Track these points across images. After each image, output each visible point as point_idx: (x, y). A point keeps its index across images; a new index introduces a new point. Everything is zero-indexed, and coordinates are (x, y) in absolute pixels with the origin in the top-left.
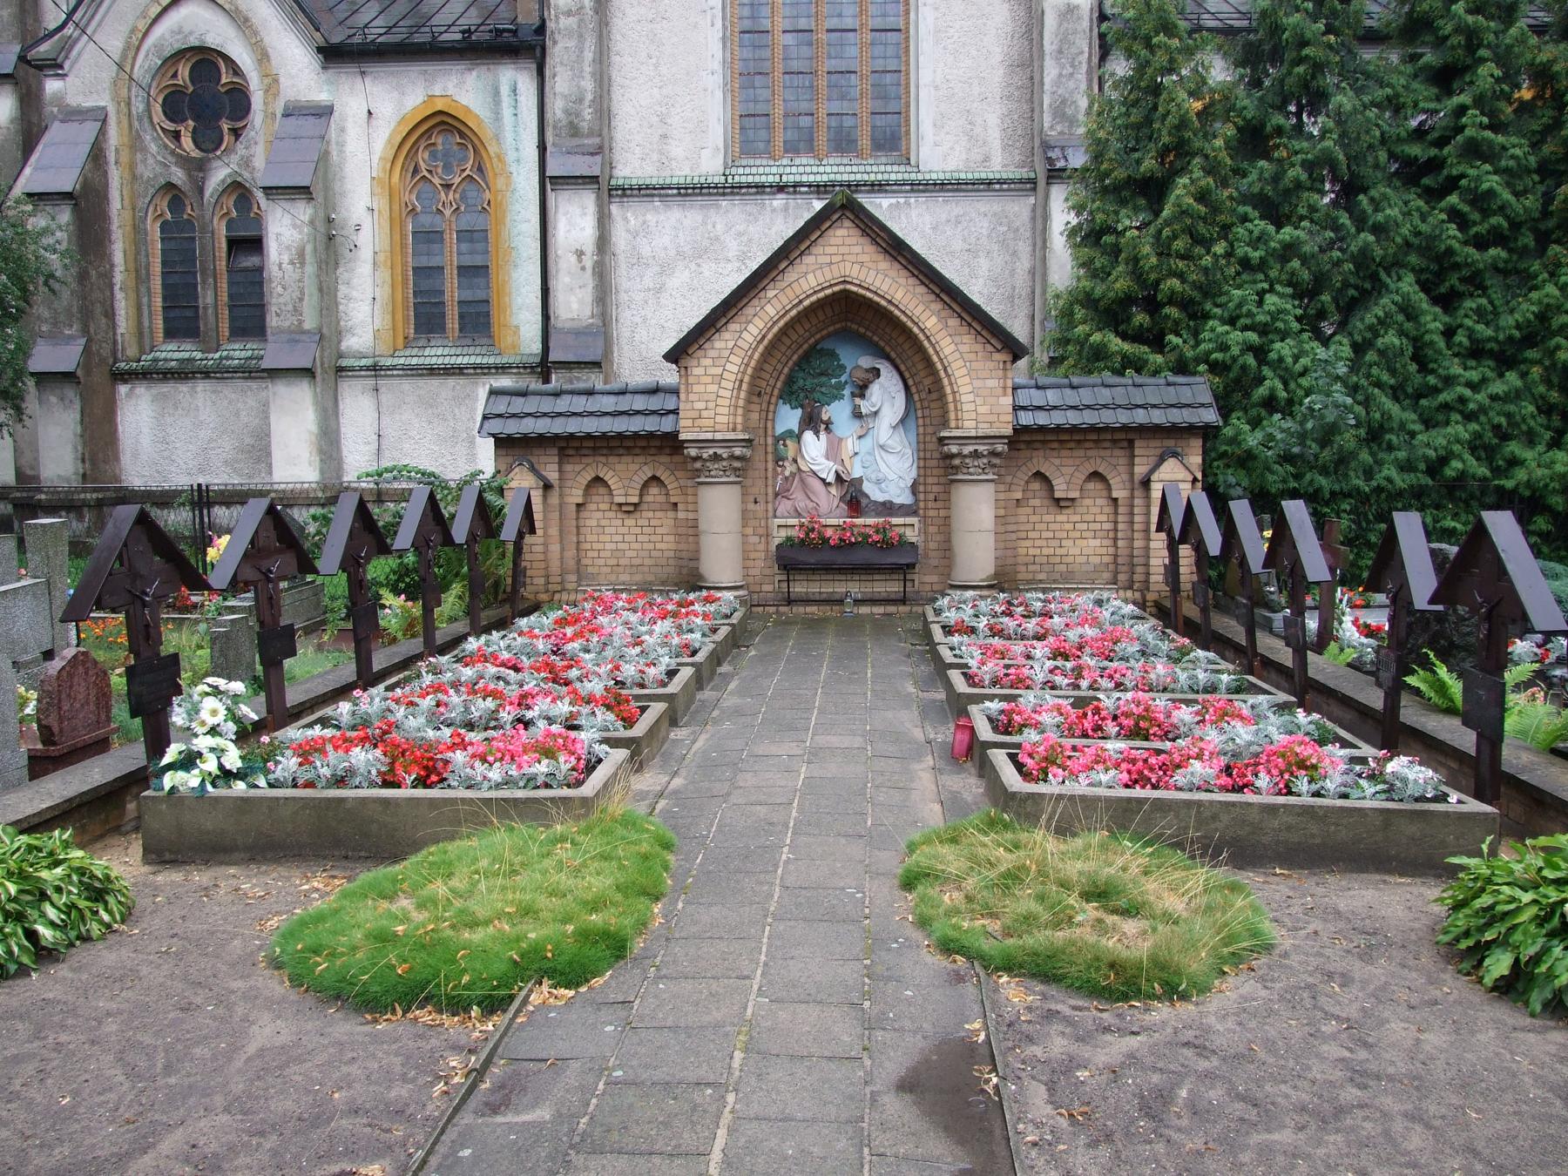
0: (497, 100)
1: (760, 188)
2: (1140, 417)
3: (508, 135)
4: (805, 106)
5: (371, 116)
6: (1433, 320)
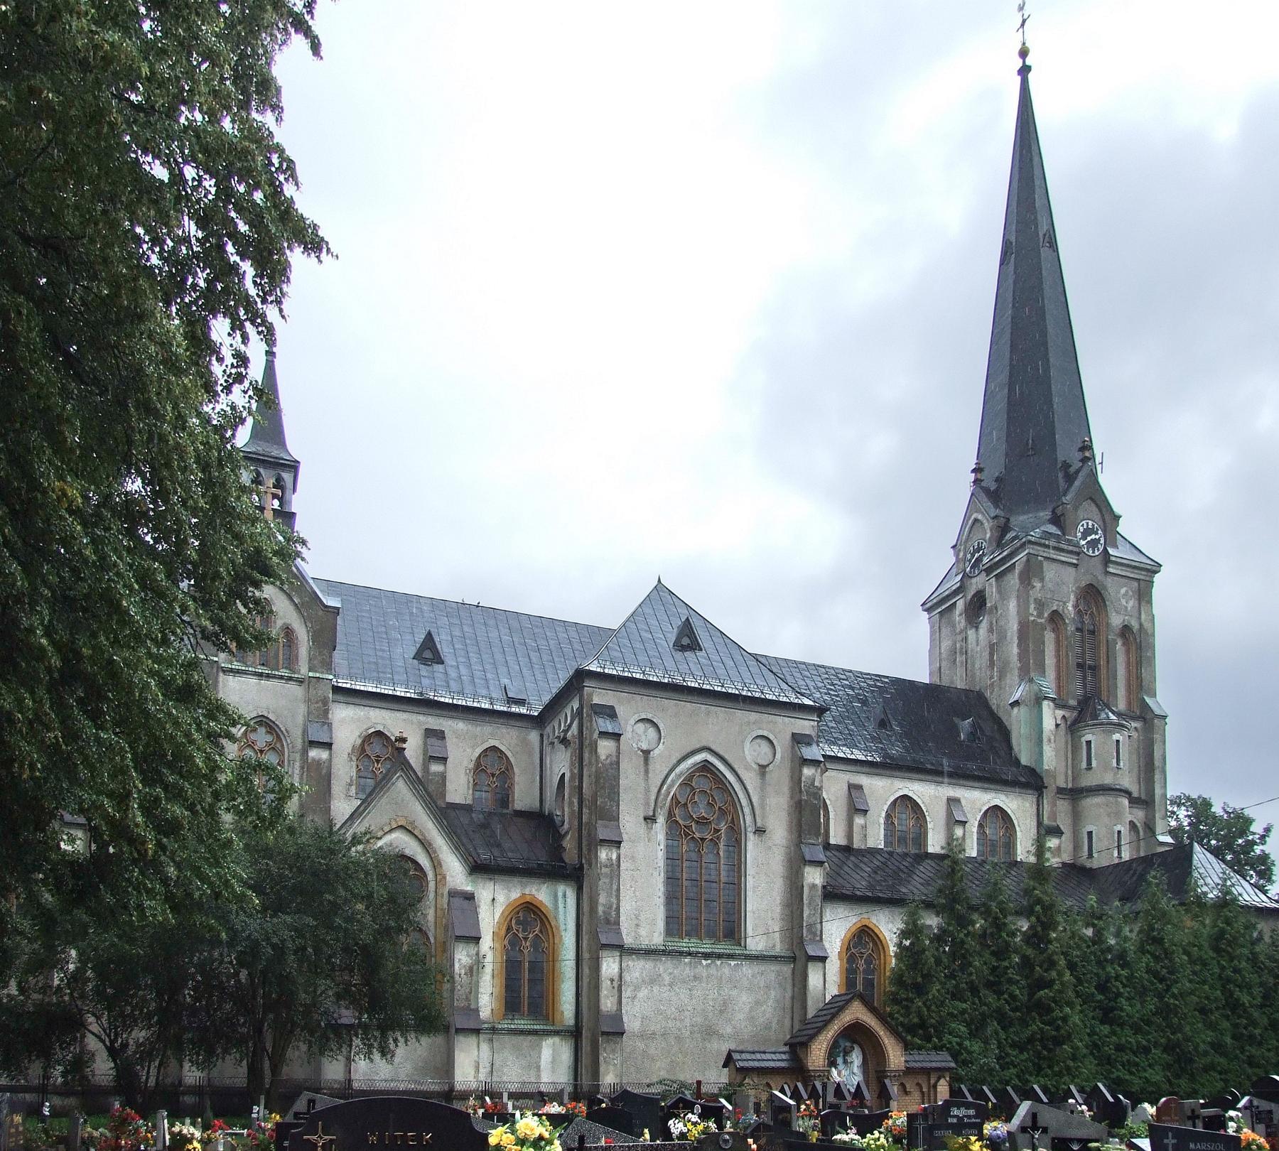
0: (559, 901)
1: (681, 953)
2: (934, 1065)
3: (561, 917)
4: (694, 915)
5: (494, 902)
6: (1002, 1035)
